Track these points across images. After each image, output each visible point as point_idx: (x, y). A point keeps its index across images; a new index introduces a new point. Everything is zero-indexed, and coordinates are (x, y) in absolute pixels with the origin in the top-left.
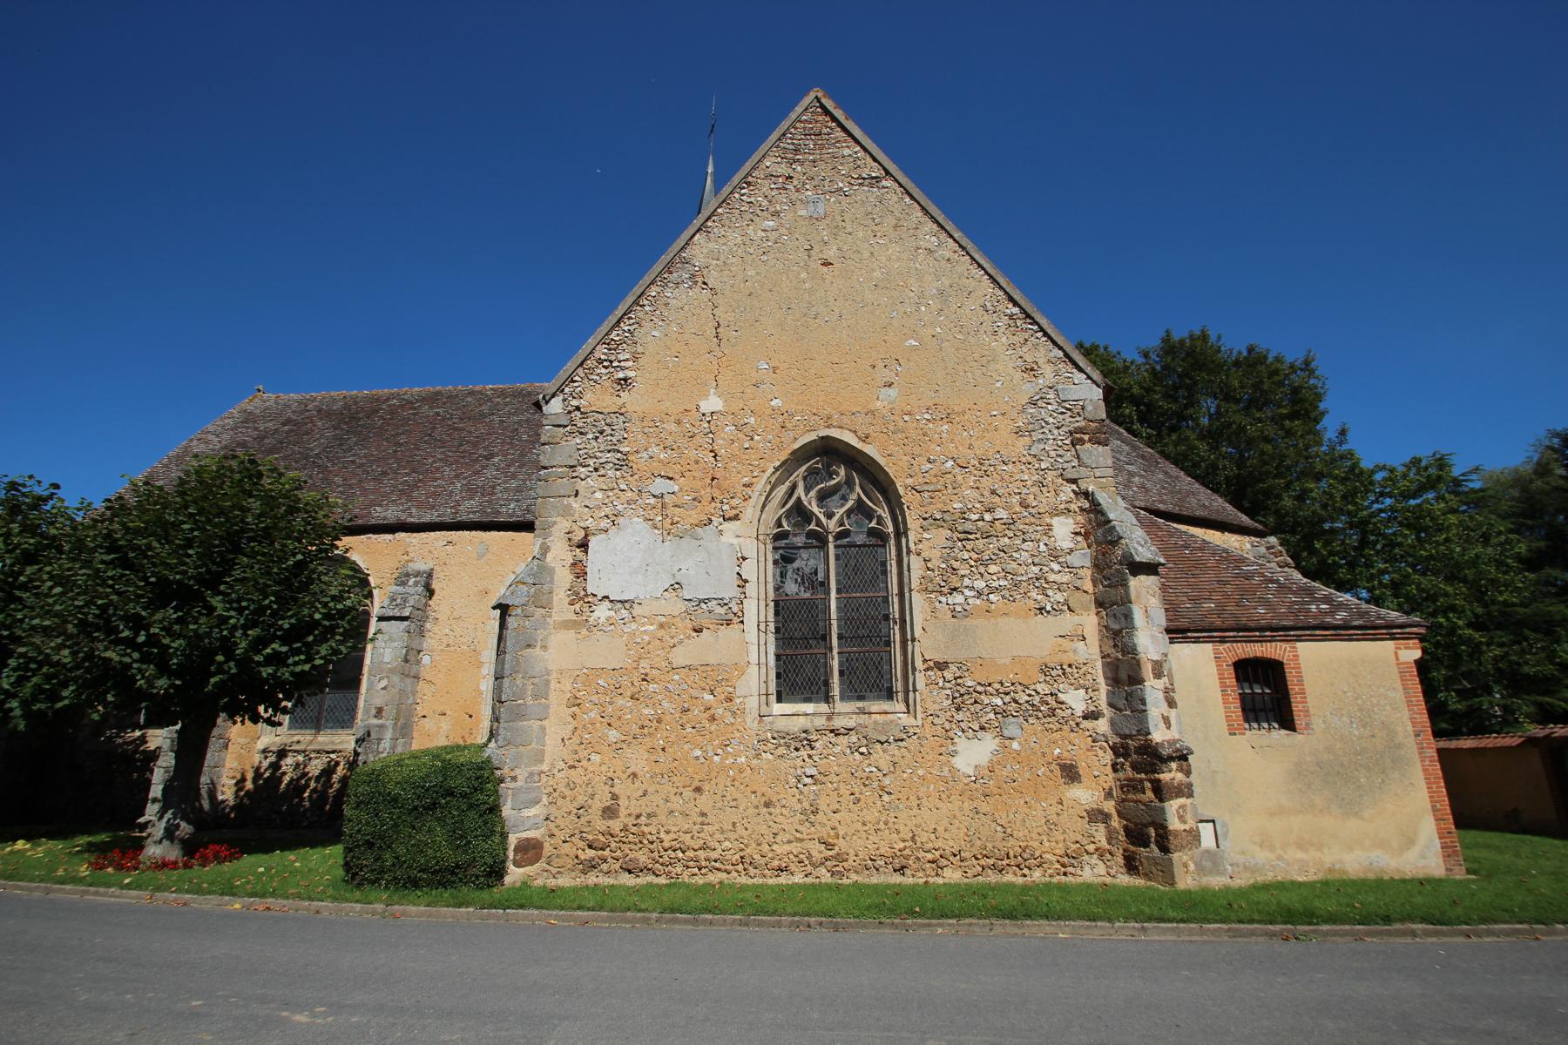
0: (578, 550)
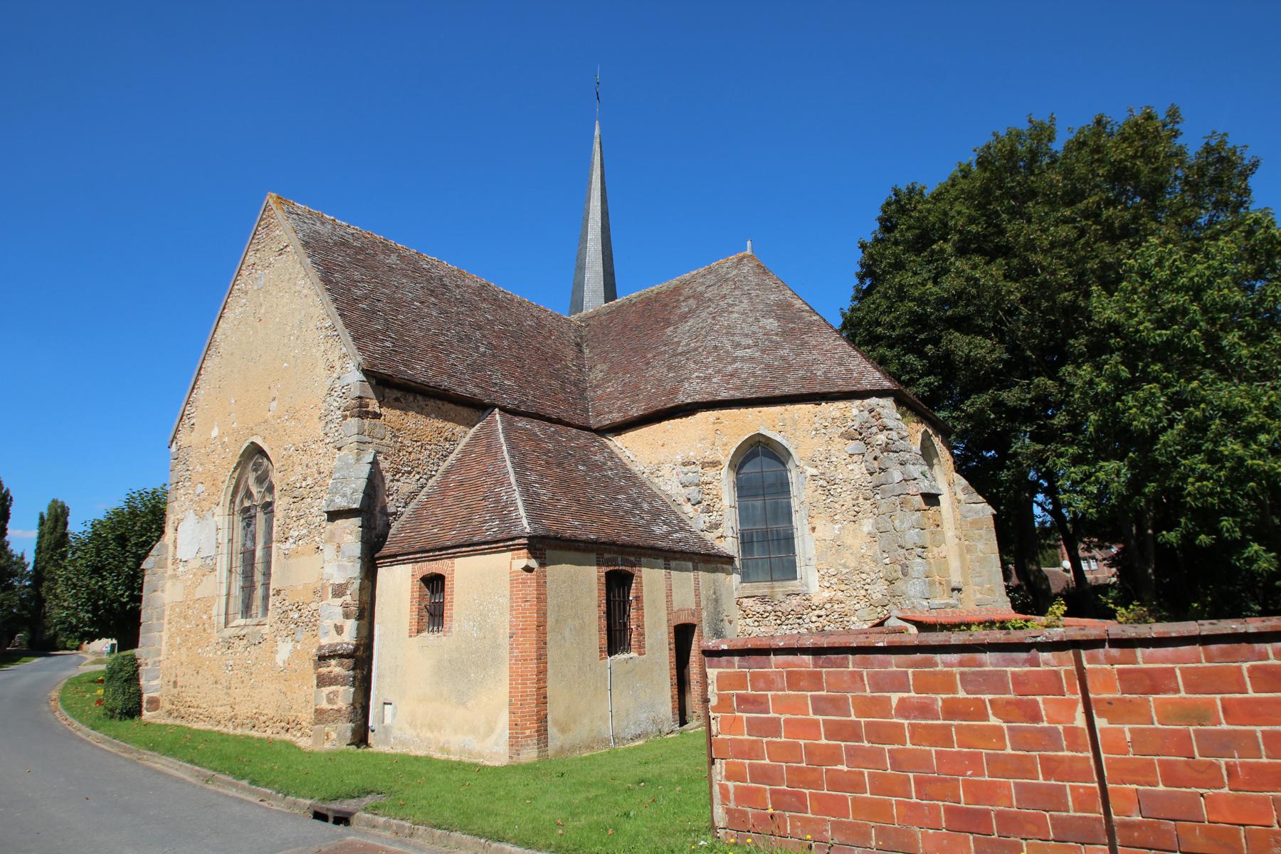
0: (839, 443)
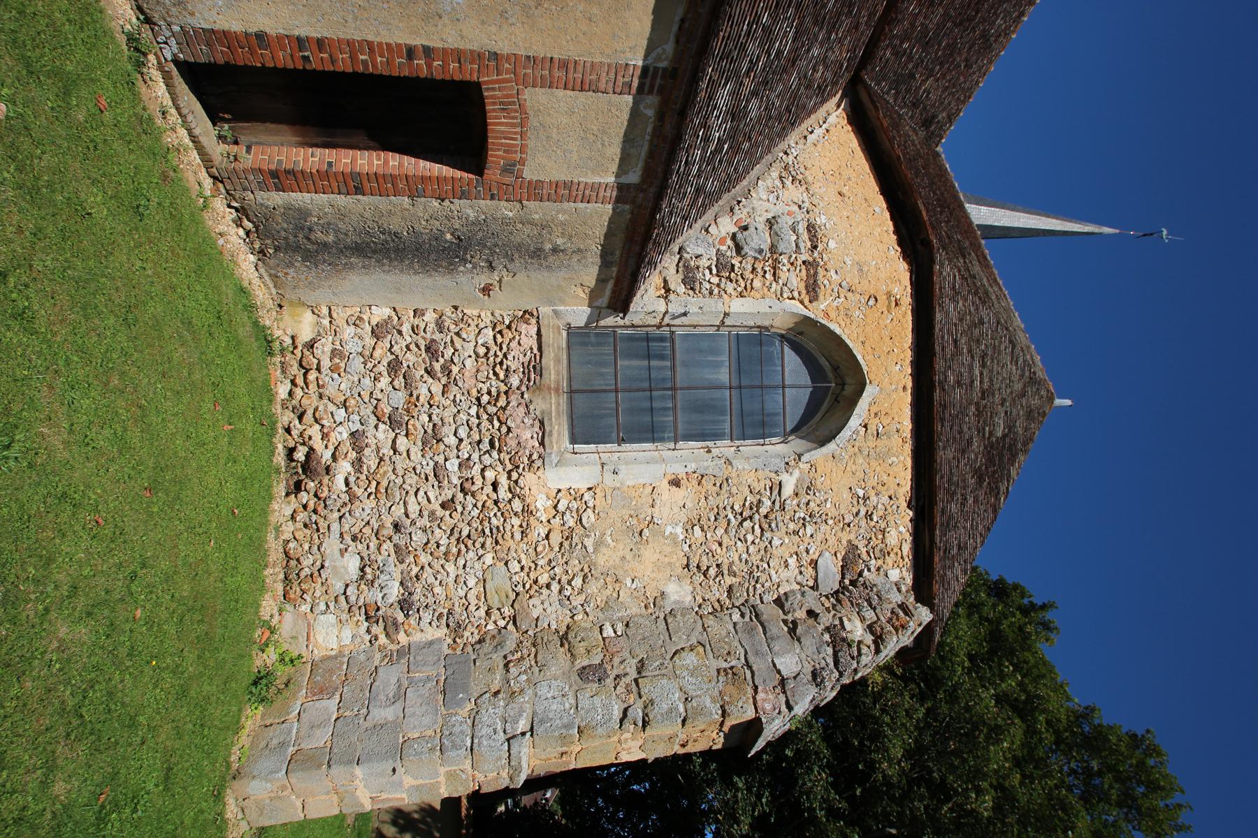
0: (838, 539)
